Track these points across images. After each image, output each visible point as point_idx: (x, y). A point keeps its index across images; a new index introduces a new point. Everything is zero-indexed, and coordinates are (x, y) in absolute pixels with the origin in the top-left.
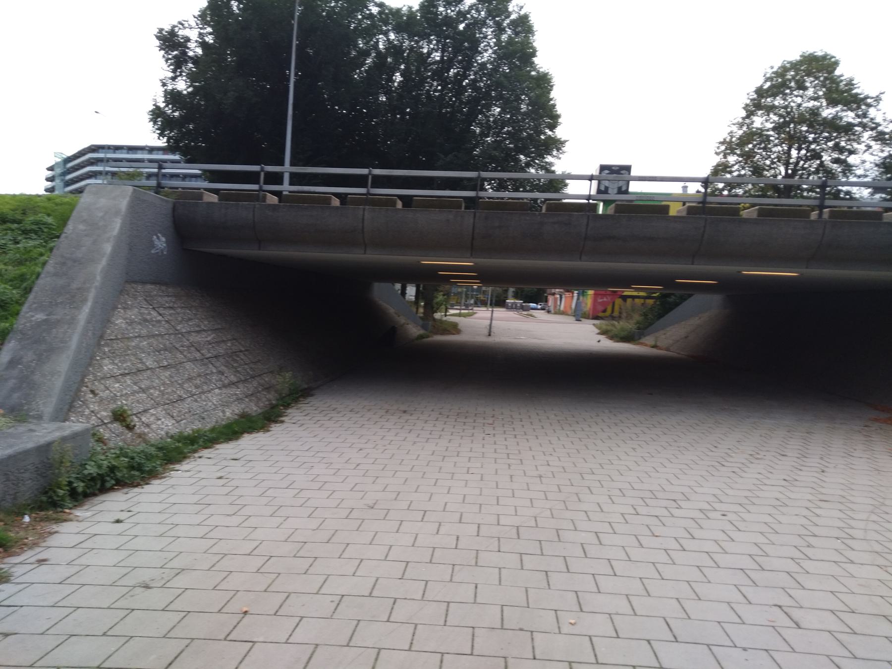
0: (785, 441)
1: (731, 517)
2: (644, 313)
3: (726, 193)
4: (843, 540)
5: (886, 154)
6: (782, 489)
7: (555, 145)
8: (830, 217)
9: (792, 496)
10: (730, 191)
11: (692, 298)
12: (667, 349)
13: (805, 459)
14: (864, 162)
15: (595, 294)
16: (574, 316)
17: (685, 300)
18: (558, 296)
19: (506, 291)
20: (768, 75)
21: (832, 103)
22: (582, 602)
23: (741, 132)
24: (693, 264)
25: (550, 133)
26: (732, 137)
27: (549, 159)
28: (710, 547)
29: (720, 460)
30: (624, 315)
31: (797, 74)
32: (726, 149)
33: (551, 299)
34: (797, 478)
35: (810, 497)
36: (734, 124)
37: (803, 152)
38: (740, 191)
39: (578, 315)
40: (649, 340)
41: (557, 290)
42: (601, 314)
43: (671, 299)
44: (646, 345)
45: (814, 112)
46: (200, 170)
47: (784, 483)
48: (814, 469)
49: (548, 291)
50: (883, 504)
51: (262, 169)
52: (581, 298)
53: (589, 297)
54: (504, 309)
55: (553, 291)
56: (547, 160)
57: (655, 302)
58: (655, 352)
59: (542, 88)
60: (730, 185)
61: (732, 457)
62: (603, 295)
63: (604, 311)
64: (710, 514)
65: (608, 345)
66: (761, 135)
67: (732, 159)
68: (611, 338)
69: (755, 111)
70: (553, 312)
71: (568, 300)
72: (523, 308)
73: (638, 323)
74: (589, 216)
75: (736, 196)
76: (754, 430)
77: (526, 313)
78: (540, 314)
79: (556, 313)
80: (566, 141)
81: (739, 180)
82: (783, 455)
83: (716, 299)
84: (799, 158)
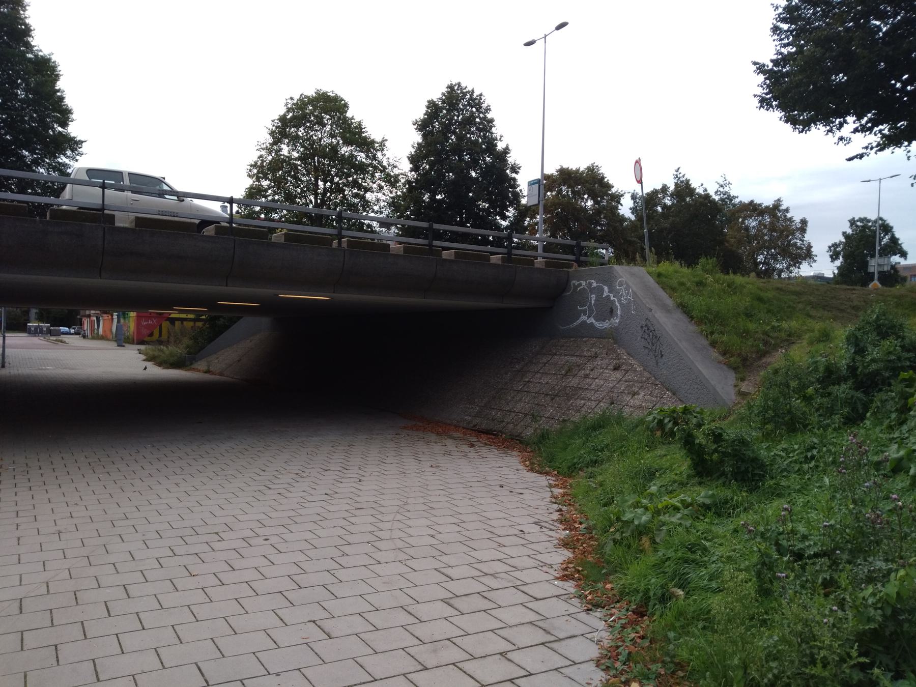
0: (329, 456)
1: (274, 540)
2: (193, 336)
3: (263, 216)
4: (373, 543)
5: (394, 195)
6: (323, 503)
7: (73, 145)
8: (348, 246)
9: (332, 508)
10: (266, 215)
11: (242, 320)
12: (221, 374)
13: (345, 471)
14: (378, 200)
15: (138, 316)
16: (116, 341)
17: (235, 322)
18: (95, 319)
19: (27, 313)
20: (289, 106)
21: (347, 142)
22: (99, 670)
23: (270, 158)
24: (334, 293)
25: (60, 129)
26: (263, 161)
27: (63, 159)
28: (251, 575)
29: (268, 483)
30: (172, 339)
31: (315, 109)
32: (258, 172)
33: (86, 321)
34: (337, 490)
35: (348, 507)
36: (263, 149)
37: (328, 184)
38: (275, 216)
39: (120, 340)
40: (202, 365)
41: (92, 312)
42: (147, 339)
43: (221, 322)
44: (199, 371)
45: (334, 149)
46: (166, 198)
47: (326, 497)
48: (352, 480)
49: (82, 312)
50: (407, 503)
51: (431, 226)
52: (122, 321)
53: (131, 320)
54: (26, 335)
55: (87, 312)
56: (59, 160)
57: (204, 325)
58: (208, 377)
59: (43, 76)
60: (267, 210)
61: (279, 478)
62: (148, 318)
63: (151, 335)
64: (252, 542)
65: (156, 372)
66: (289, 164)
67: (265, 183)
68: (160, 364)
69: (281, 138)
70: (90, 336)
71: (110, 322)
72: (50, 333)
73: (188, 347)
74: (104, 228)
75: (273, 220)
76: (302, 449)
77: (54, 339)
78: (74, 340)
79: (93, 338)
80: (81, 142)
81: (272, 205)
82: (326, 470)
83: (264, 322)
84: (325, 190)
